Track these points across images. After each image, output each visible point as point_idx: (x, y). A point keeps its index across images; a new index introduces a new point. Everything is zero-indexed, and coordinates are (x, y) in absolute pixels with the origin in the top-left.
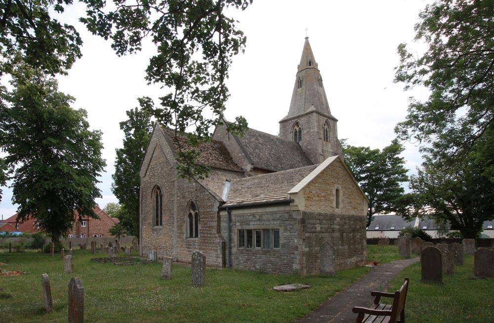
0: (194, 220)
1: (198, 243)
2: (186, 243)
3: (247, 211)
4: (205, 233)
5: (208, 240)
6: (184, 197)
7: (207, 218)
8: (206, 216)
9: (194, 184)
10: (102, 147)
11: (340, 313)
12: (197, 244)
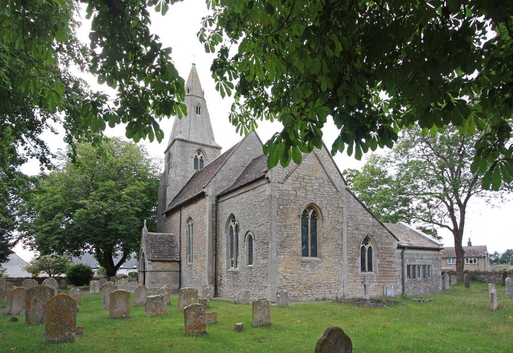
0: (366, 253)
1: (376, 277)
2: (362, 278)
3: (414, 252)
4: (384, 268)
5: (388, 274)
6: (357, 229)
7: (385, 253)
8: (384, 252)
9: (371, 219)
10: (217, 45)
11: (237, 324)
12: (375, 278)
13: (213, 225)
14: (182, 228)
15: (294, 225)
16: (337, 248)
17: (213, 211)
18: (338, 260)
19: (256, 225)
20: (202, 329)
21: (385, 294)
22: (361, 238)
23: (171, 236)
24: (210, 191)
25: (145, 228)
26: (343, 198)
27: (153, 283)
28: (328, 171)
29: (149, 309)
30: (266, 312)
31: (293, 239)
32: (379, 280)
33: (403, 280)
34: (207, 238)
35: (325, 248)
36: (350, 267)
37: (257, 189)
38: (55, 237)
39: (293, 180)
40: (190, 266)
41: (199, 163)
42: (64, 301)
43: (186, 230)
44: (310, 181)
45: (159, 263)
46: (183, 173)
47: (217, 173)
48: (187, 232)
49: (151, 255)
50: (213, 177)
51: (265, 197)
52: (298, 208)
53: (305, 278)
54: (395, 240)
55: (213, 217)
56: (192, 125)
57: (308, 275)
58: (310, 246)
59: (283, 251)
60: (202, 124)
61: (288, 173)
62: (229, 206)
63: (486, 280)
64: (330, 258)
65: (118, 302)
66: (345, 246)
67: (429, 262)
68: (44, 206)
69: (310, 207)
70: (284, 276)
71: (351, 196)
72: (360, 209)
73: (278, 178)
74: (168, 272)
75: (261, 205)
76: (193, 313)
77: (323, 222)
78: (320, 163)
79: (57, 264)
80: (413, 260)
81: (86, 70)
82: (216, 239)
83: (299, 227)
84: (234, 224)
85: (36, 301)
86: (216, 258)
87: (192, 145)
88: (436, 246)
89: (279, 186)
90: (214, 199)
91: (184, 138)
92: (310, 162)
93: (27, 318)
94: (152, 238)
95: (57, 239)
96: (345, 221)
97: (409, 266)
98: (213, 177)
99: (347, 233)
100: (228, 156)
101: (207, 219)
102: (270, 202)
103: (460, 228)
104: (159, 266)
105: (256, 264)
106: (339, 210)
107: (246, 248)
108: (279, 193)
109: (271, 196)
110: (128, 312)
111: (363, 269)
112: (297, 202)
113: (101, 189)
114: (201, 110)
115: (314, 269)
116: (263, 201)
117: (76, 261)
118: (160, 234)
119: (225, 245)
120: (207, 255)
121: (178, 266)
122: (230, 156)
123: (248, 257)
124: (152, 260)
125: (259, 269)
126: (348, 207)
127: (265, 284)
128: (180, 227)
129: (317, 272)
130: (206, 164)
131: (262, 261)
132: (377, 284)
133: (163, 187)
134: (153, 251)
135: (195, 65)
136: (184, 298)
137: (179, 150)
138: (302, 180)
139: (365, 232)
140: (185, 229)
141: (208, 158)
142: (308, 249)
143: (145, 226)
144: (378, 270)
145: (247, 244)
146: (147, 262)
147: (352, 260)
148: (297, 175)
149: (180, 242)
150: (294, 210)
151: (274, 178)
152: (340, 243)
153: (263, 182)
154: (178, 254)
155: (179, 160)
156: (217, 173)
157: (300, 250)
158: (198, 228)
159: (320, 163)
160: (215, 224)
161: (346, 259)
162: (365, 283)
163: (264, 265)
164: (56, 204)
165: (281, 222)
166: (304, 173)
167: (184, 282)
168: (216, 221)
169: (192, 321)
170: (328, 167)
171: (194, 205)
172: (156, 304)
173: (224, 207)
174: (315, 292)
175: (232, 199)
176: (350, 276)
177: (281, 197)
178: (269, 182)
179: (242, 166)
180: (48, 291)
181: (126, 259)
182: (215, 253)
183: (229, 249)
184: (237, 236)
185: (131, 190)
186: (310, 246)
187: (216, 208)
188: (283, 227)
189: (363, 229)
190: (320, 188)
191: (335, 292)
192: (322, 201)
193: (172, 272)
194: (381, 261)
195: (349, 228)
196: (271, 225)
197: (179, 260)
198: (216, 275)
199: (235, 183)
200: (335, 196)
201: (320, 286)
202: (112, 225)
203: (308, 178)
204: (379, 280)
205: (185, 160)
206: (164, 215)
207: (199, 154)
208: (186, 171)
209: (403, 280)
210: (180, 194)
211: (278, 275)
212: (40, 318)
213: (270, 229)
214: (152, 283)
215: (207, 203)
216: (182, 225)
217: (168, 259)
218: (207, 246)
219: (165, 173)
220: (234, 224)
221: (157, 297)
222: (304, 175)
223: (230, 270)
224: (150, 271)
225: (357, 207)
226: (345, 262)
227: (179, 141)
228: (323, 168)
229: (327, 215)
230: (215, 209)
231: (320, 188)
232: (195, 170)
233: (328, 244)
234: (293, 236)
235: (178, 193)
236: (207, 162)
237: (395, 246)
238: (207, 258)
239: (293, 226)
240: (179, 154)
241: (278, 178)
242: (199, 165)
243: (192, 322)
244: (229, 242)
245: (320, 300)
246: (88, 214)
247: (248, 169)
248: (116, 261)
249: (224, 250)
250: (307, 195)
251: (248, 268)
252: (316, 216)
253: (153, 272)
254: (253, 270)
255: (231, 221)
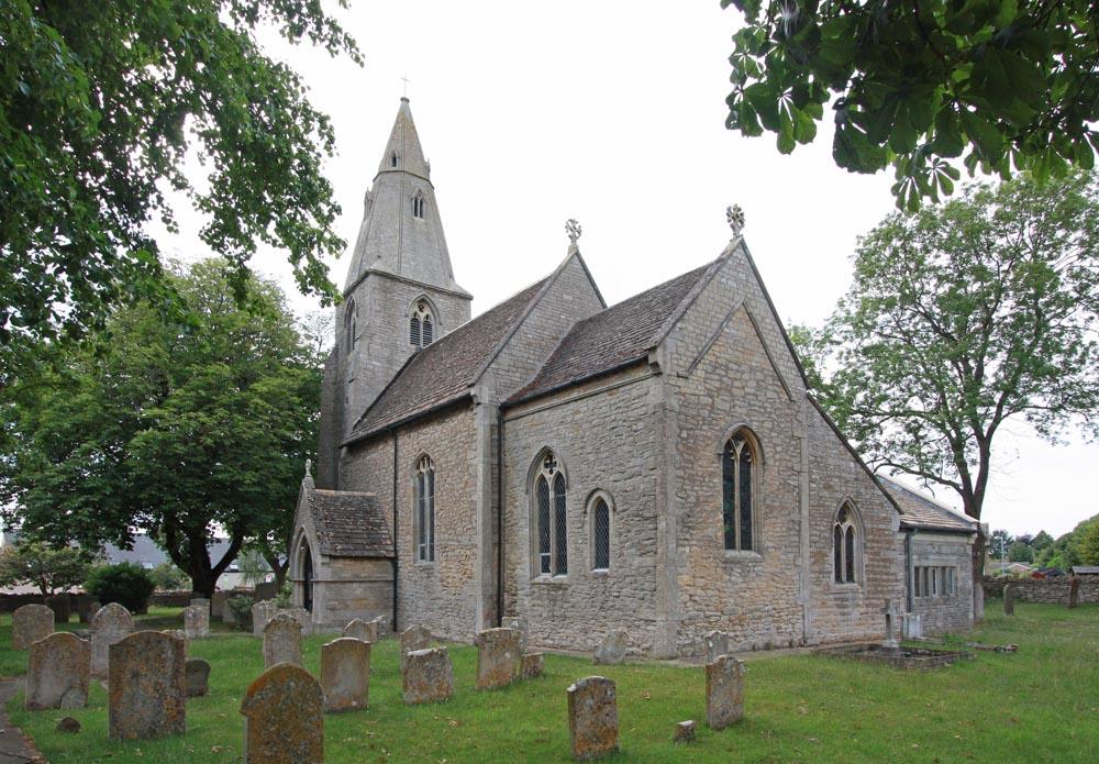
1: (863, 593)
6: (828, 487)
7: (878, 542)
9: (852, 465)
11: (683, 723)
12: (861, 596)
13: (492, 474)
14: (399, 481)
15: (710, 476)
16: (790, 529)
17: (492, 440)
18: (791, 556)
19: (618, 476)
20: (610, 741)
21: (905, 632)
22: (835, 507)
23: (369, 500)
24: (484, 394)
25: (308, 478)
26: (800, 417)
27: (333, 609)
28: (774, 355)
29: (415, 684)
30: (735, 691)
31: (707, 508)
32: (867, 602)
33: (909, 599)
34: (480, 506)
35: (769, 531)
36: (814, 572)
37: (621, 389)
38: (82, 499)
39: (707, 372)
40: (428, 571)
42: (292, 684)
43: (411, 484)
45: (347, 562)
46: (386, 353)
47: (500, 351)
48: (414, 489)
49: (327, 545)
50: (492, 361)
51: (644, 408)
52: (717, 436)
53: (732, 600)
54: (896, 512)
55: (492, 455)
56: (406, 241)
57: (737, 592)
58: (740, 530)
59: (688, 536)
60: (428, 239)
61: (695, 355)
62: (533, 431)
63: (1030, 596)
64: (778, 553)
65: (339, 669)
66: (805, 524)
67: (952, 561)
68: (50, 420)
69: (739, 435)
70: (691, 596)
71: (817, 414)
72: (834, 443)
73: (678, 365)
74: (368, 584)
75: (634, 427)
76: (590, 702)
77: (765, 470)
78: (759, 334)
79: (63, 563)
80: (923, 555)
81: (310, 33)
82: (499, 508)
83: (718, 481)
84: (551, 472)
85: (136, 675)
86: (499, 550)
87: (406, 287)
88: (964, 527)
89: (679, 384)
90: (495, 412)
91: (389, 271)
92: (738, 330)
93: (114, 719)
94: (328, 503)
95: (86, 504)
96: (805, 468)
97: (917, 569)
98: (492, 361)
100: (525, 313)
101: (478, 461)
102: (661, 421)
103: (977, 488)
104: (348, 569)
105: (621, 567)
106: (794, 442)
107: (589, 527)
108: (680, 400)
109: (663, 406)
110: (366, 694)
111: (838, 579)
112: (714, 422)
113: (194, 382)
114: (424, 209)
115: (747, 579)
116: (639, 420)
117: (112, 556)
118: (343, 493)
119: (523, 523)
120: (480, 544)
121: (391, 570)
122: (529, 313)
123: (594, 549)
124: (331, 557)
125: (627, 580)
126: (811, 437)
127: (645, 613)
128: (396, 478)
129: (753, 585)
130: (439, 334)
131: (637, 561)
132: (863, 610)
133: (334, 384)
134: (332, 534)
135: (408, 101)
136: (490, 654)
137: (378, 297)
138: (724, 373)
139: (843, 493)
140: (408, 484)
141: (442, 321)
142: (734, 531)
143: (308, 474)
144: (865, 579)
145: (590, 519)
146: (317, 559)
147: (818, 557)
149: (396, 512)
150: (710, 442)
151: (669, 365)
152: (795, 517)
153: (641, 373)
154: (389, 542)
155: (378, 321)
156: (500, 351)
157: (720, 534)
158: (449, 480)
159: (759, 334)
160: (497, 471)
161: (807, 555)
162: (889, 612)
163: (644, 570)
164: (80, 417)
165: (684, 469)
166: (727, 357)
167: (407, 608)
168: (499, 464)
169: (588, 722)
170: (774, 344)
171: (439, 428)
172: (429, 671)
173: (520, 433)
174: (750, 632)
175: (546, 413)
176: (815, 593)
177: (683, 409)
178: (659, 374)
179: (553, 338)
180: (167, 644)
181: (240, 553)
182: (497, 539)
183: (537, 532)
184: (561, 503)
185: (272, 388)
186: (740, 530)
187: (500, 433)
188: (687, 482)
189: (837, 488)
190: (758, 393)
191: (788, 630)
192: (763, 422)
193: (376, 585)
194: (870, 559)
195: (814, 485)
196: (664, 475)
197: (392, 555)
198: (499, 592)
199: (540, 378)
200: (788, 411)
201: (760, 618)
202: (221, 470)
203: (735, 367)
204: (867, 602)
205: (390, 322)
206: (344, 450)
207: (421, 310)
208: (394, 347)
209: (909, 599)
210: (383, 401)
211: (680, 593)
212: (147, 720)
213: (663, 485)
214: (331, 609)
215: (479, 422)
216: (400, 474)
217: (366, 554)
218: (480, 528)
219: (336, 350)
220: (551, 472)
221: (431, 654)
223: (537, 580)
224: (327, 582)
225: (827, 438)
226: (806, 562)
227: (377, 278)
228: (765, 347)
229: (771, 454)
230: (496, 437)
231: (758, 393)
232: (414, 347)
233: (773, 520)
234: (707, 501)
235: (375, 398)
236: (439, 327)
237: (895, 526)
238: (479, 552)
239: (707, 480)
240: (378, 308)
241: (678, 365)
242: (422, 335)
243: (586, 726)
244: (537, 515)
245: (759, 649)
246: (165, 443)
247: (568, 344)
248: (215, 555)
249: (523, 532)
250: (734, 406)
251: (596, 577)
252: (749, 457)
253: (333, 585)
254: (611, 581)
255: (542, 466)
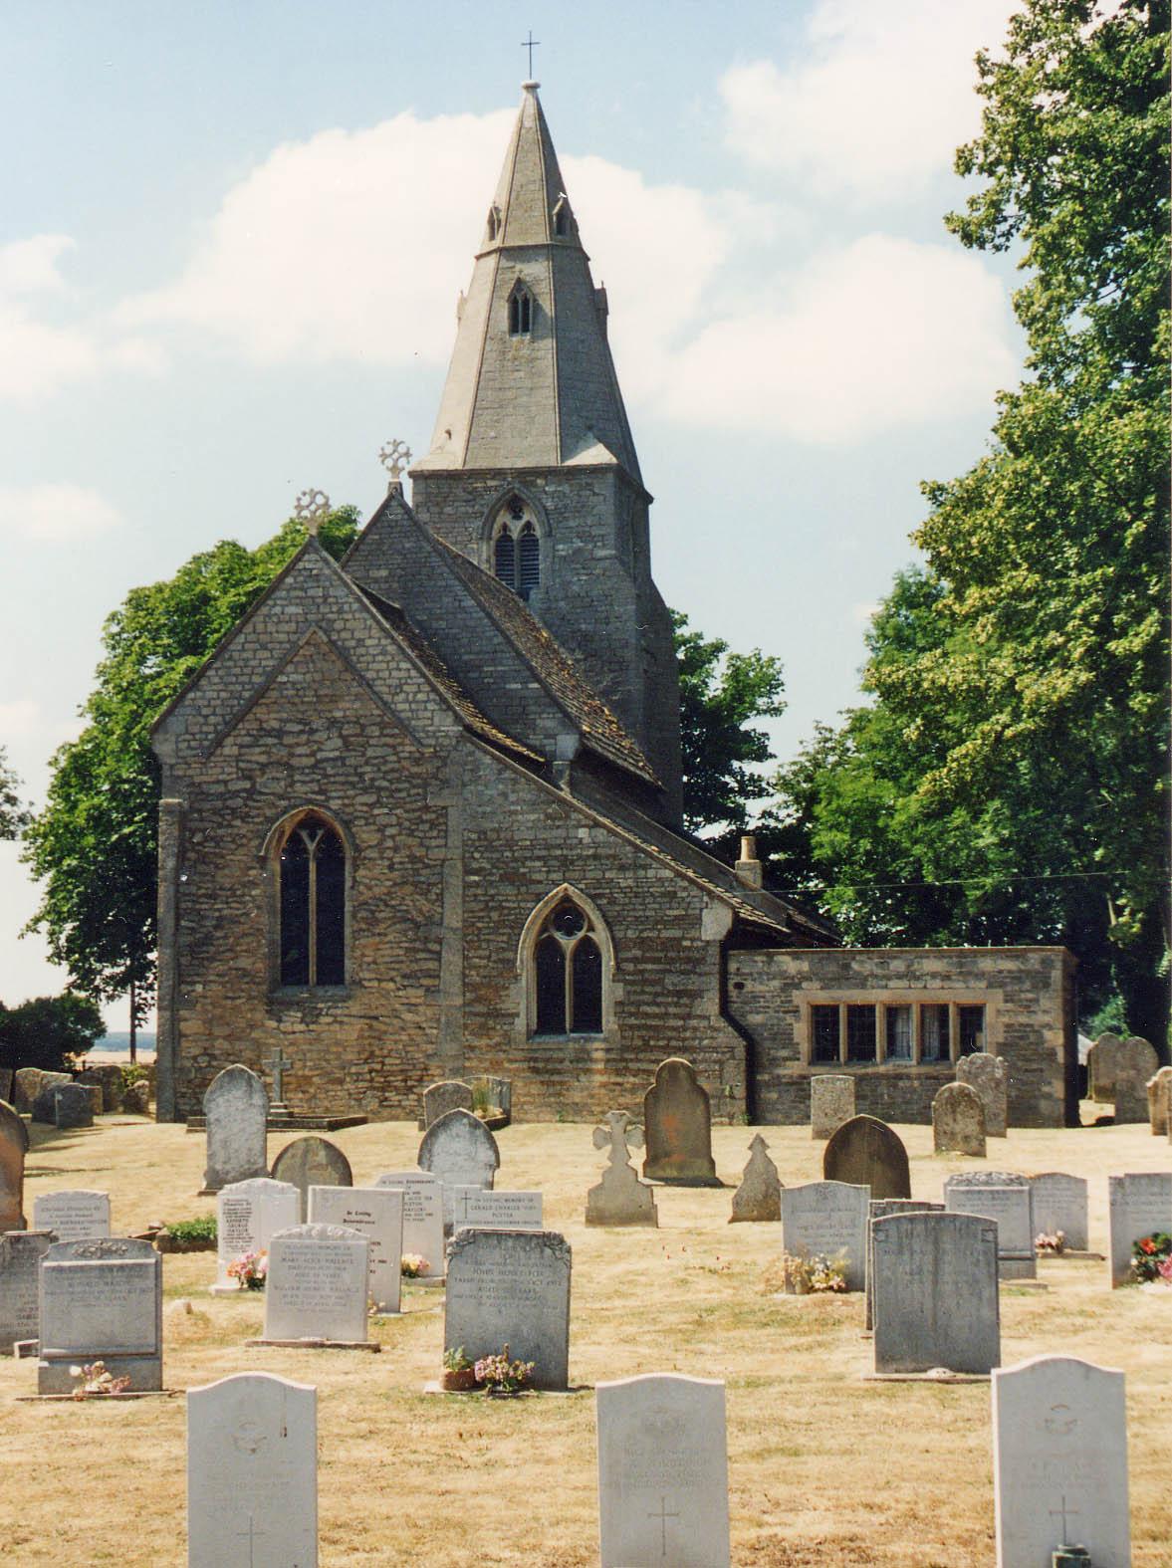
41: (516, 553)
44: (304, 737)
69: (311, 823)
99: (464, 895)
148: (255, 725)
150: (244, 841)
222: (281, 720)
